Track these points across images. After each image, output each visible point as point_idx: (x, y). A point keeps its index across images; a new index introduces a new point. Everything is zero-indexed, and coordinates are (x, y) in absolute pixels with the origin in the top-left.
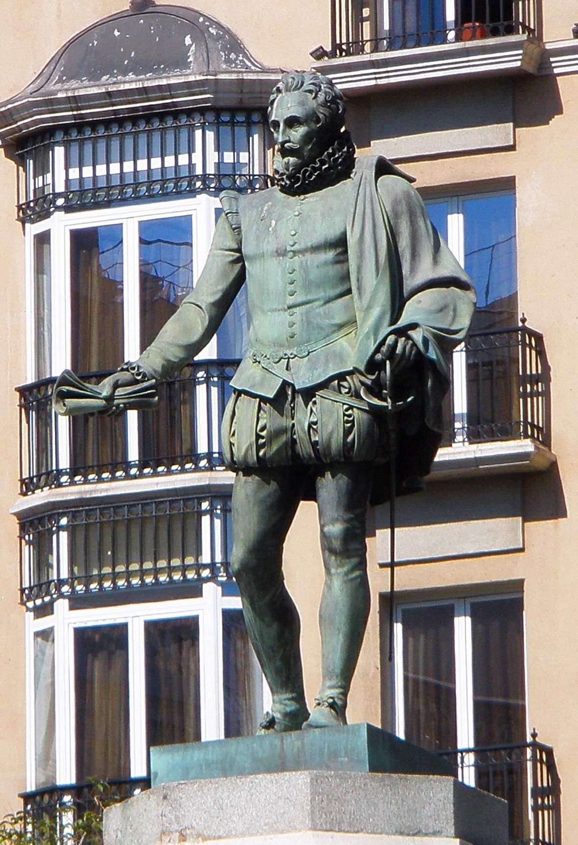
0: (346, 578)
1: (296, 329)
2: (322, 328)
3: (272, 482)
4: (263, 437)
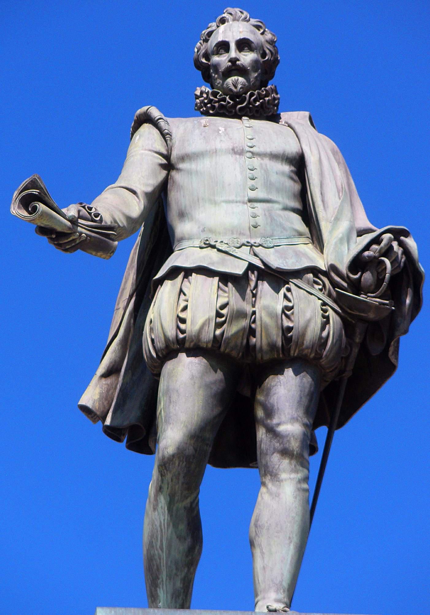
0: (299, 486)
1: (260, 220)
2: (284, 229)
3: (219, 370)
4: (221, 316)
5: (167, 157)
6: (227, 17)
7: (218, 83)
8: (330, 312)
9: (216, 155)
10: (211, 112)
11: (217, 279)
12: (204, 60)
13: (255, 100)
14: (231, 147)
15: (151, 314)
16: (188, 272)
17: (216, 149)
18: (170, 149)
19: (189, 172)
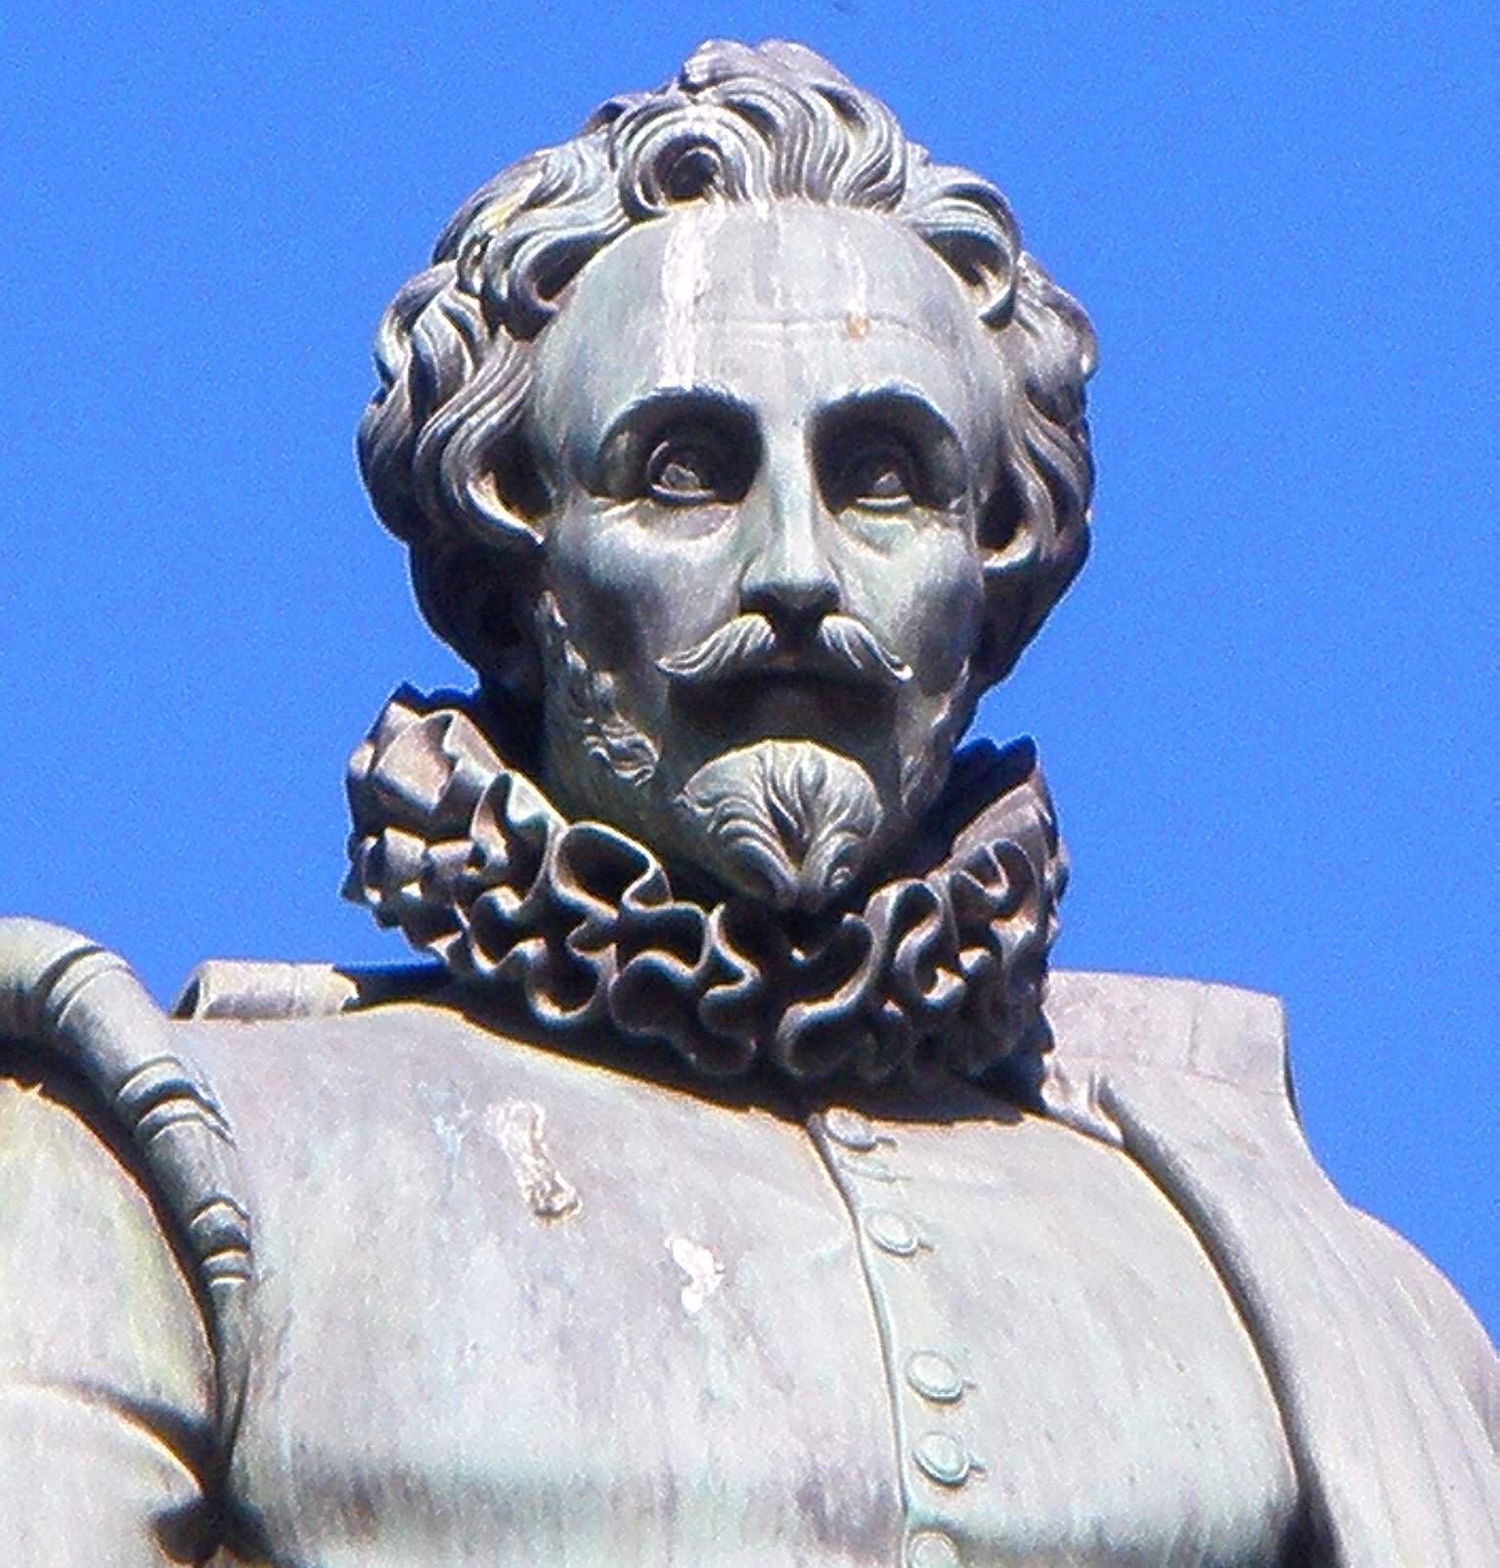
5: (206, 1446)
6: (729, 144)
7: (621, 756)
9: (671, 1539)
10: (548, 1010)
12: (487, 500)
13: (939, 954)
14: (792, 1477)
17: (670, 1481)
18: (225, 1374)
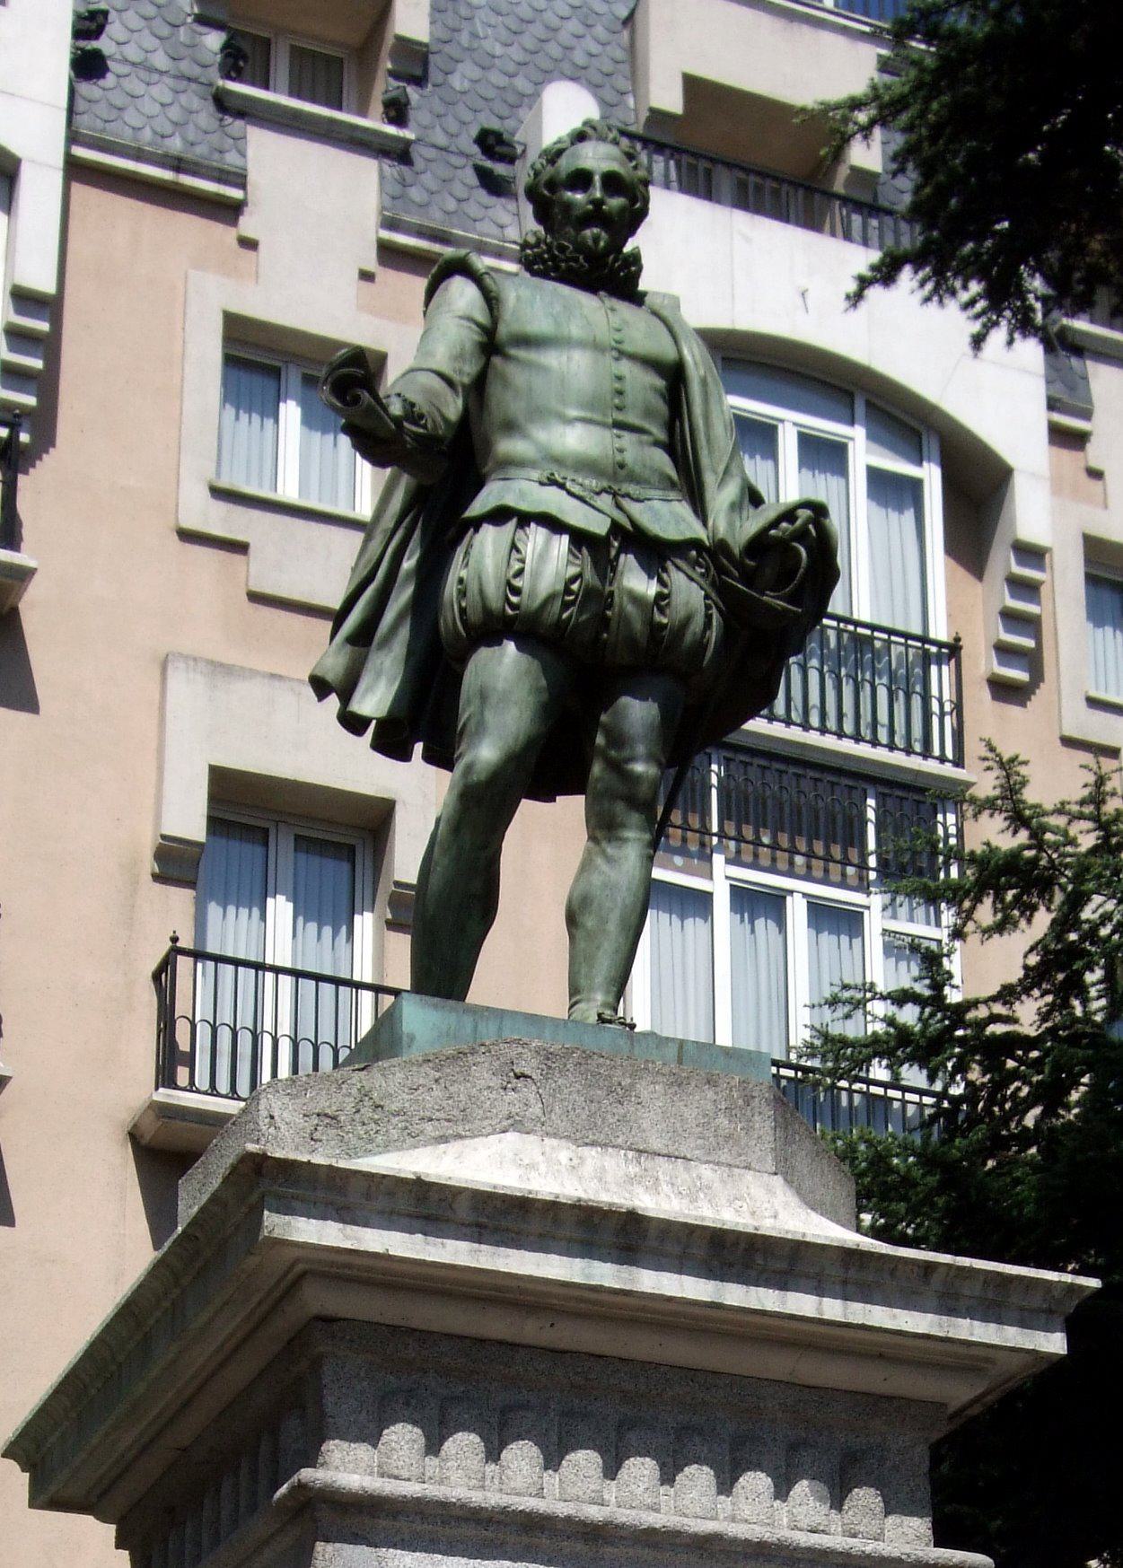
8: (714, 611)
11: (565, 539)
15: (457, 571)
16: (525, 519)
19: (529, 365)
